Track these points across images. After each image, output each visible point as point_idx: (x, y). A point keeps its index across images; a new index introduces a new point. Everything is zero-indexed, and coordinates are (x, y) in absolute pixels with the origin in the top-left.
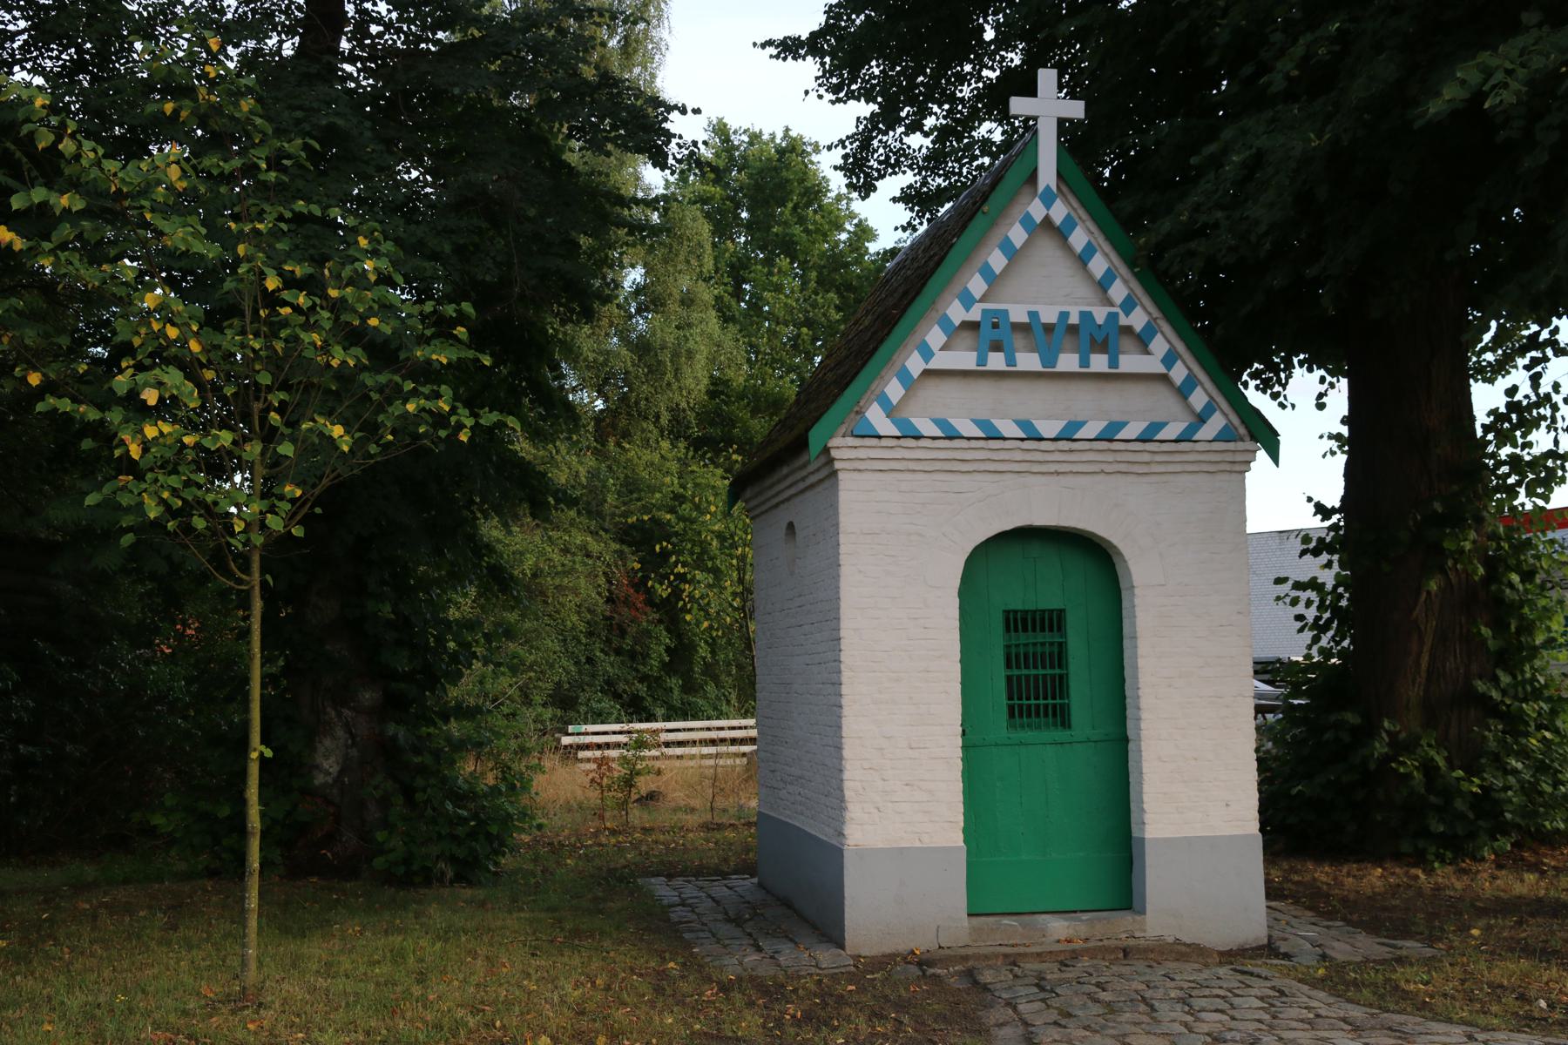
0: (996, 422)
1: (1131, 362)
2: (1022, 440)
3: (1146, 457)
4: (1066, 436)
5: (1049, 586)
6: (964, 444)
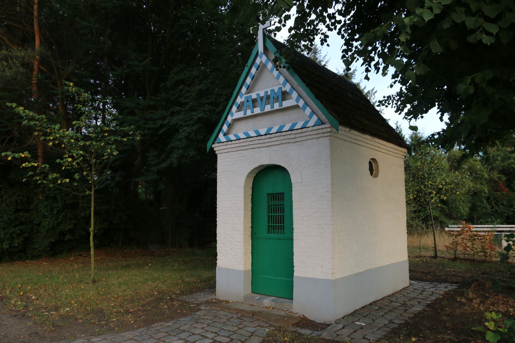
1: (286, 104)
2: (235, 140)
3: (293, 136)
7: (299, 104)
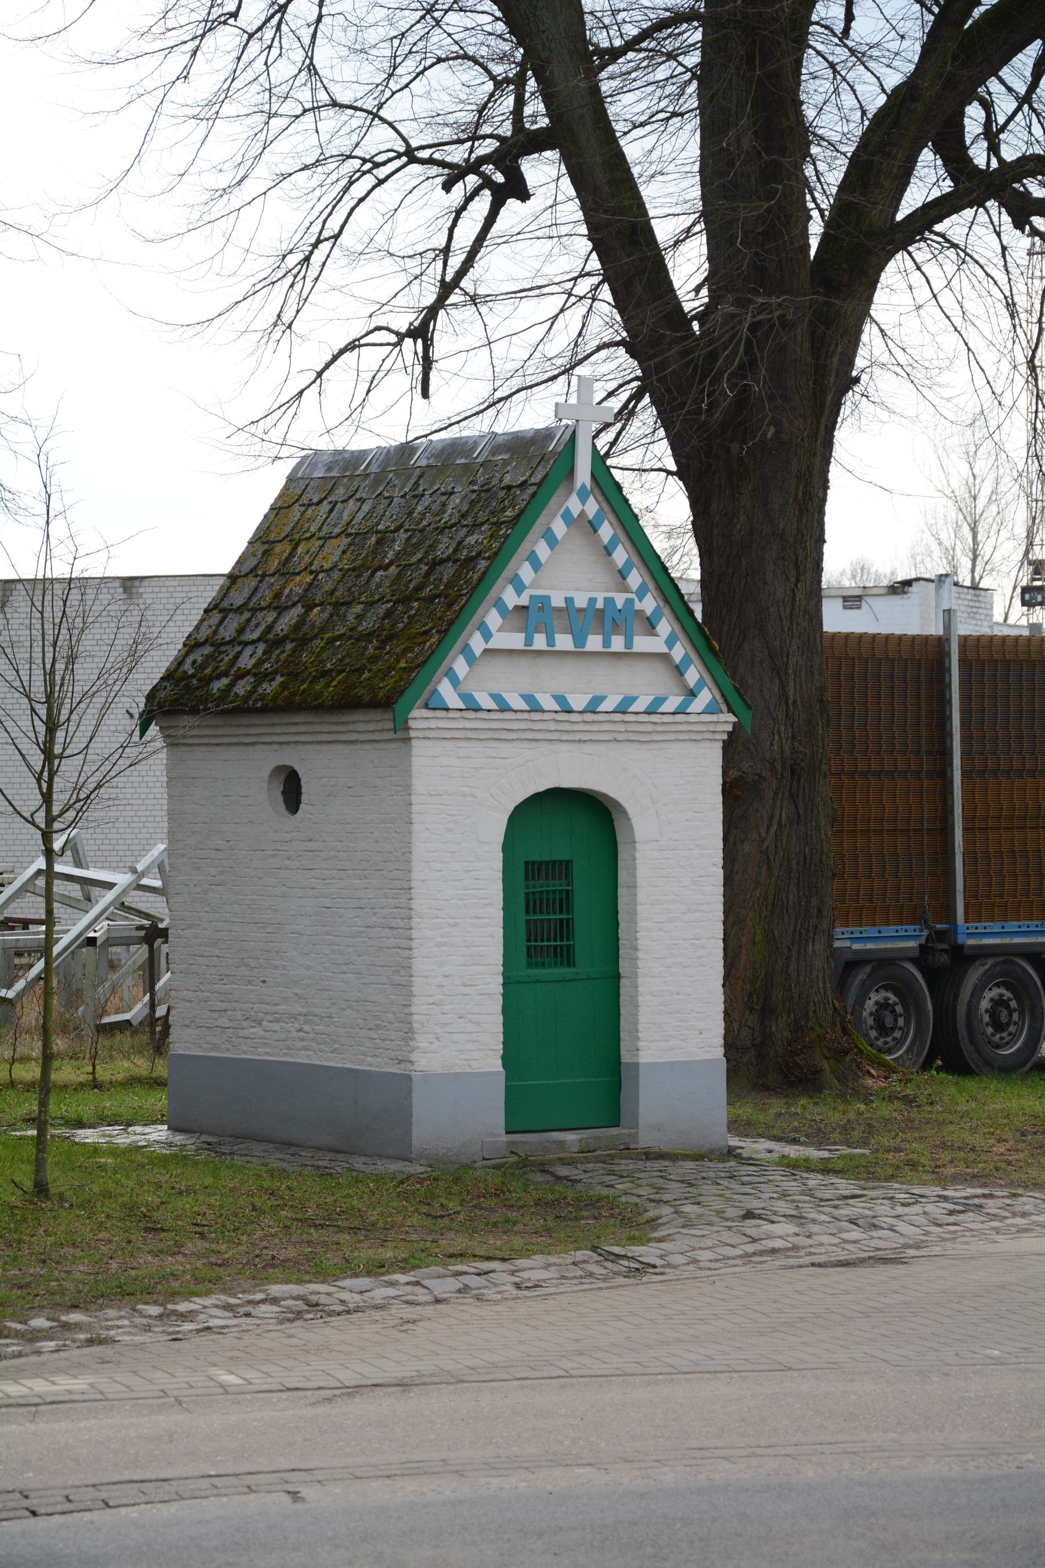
0: (477, 695)
1: (642, 643)
3: (649, 728)
4: (591, 709)
5: (555, 844)
6: (485, 715)
7: (672, 653)
